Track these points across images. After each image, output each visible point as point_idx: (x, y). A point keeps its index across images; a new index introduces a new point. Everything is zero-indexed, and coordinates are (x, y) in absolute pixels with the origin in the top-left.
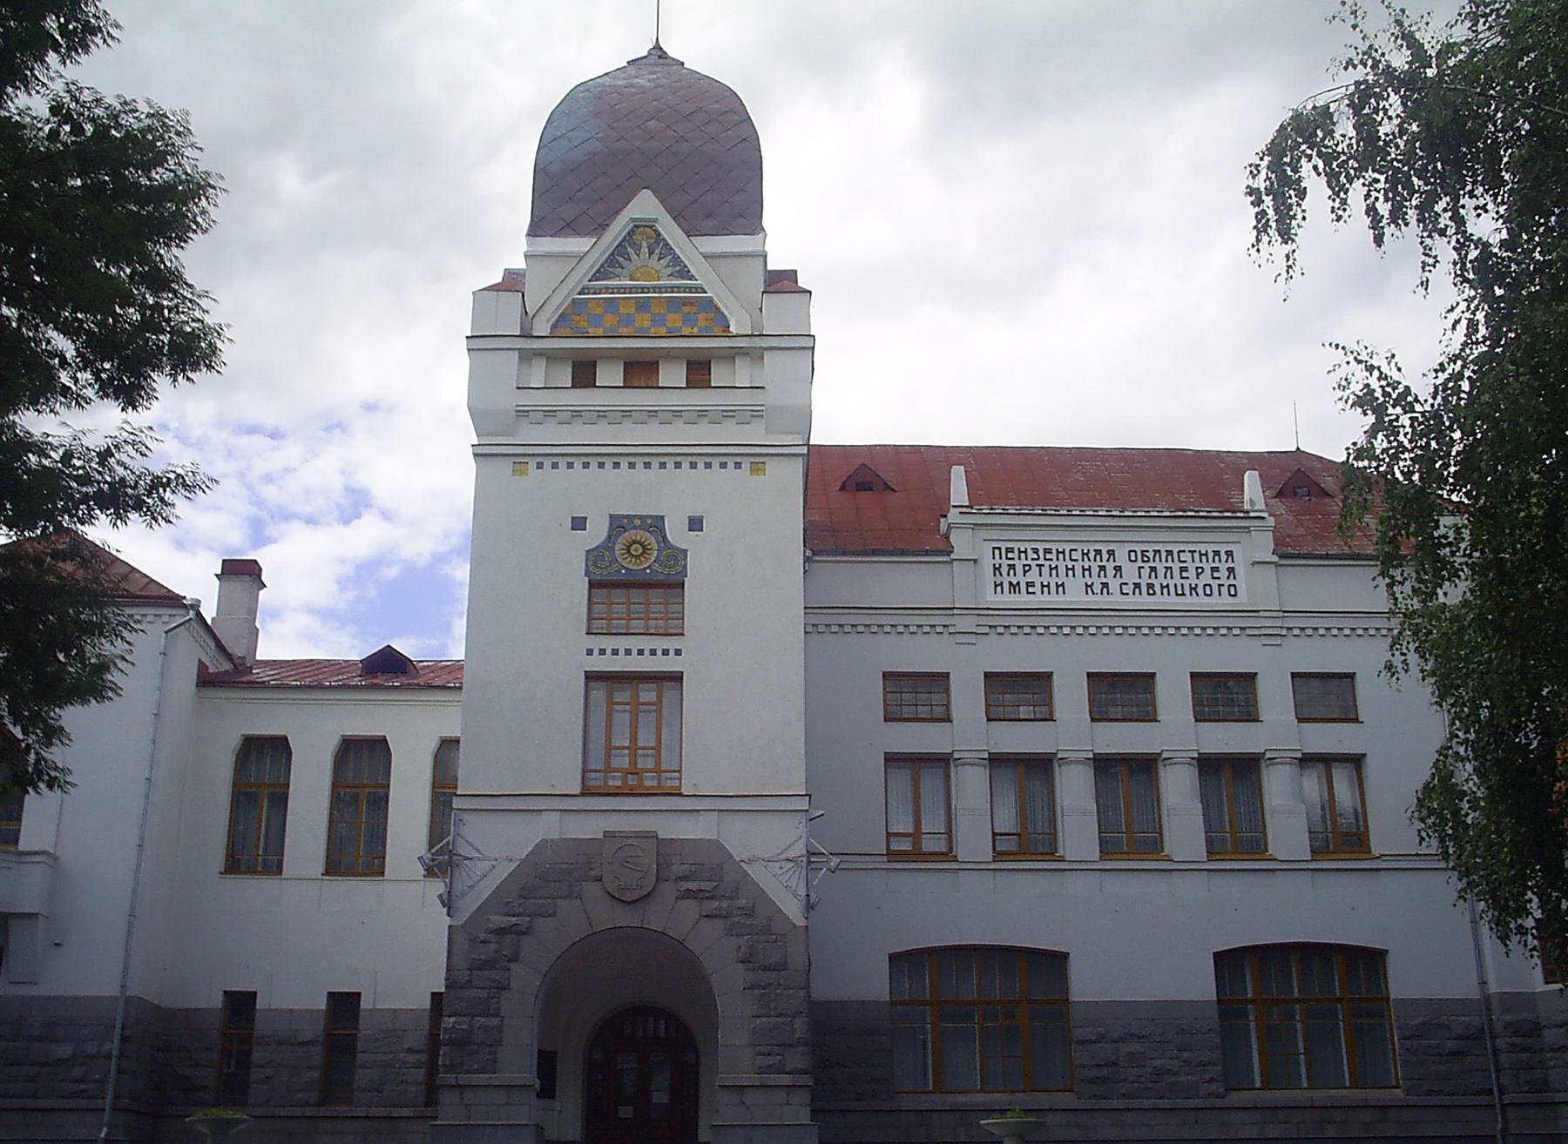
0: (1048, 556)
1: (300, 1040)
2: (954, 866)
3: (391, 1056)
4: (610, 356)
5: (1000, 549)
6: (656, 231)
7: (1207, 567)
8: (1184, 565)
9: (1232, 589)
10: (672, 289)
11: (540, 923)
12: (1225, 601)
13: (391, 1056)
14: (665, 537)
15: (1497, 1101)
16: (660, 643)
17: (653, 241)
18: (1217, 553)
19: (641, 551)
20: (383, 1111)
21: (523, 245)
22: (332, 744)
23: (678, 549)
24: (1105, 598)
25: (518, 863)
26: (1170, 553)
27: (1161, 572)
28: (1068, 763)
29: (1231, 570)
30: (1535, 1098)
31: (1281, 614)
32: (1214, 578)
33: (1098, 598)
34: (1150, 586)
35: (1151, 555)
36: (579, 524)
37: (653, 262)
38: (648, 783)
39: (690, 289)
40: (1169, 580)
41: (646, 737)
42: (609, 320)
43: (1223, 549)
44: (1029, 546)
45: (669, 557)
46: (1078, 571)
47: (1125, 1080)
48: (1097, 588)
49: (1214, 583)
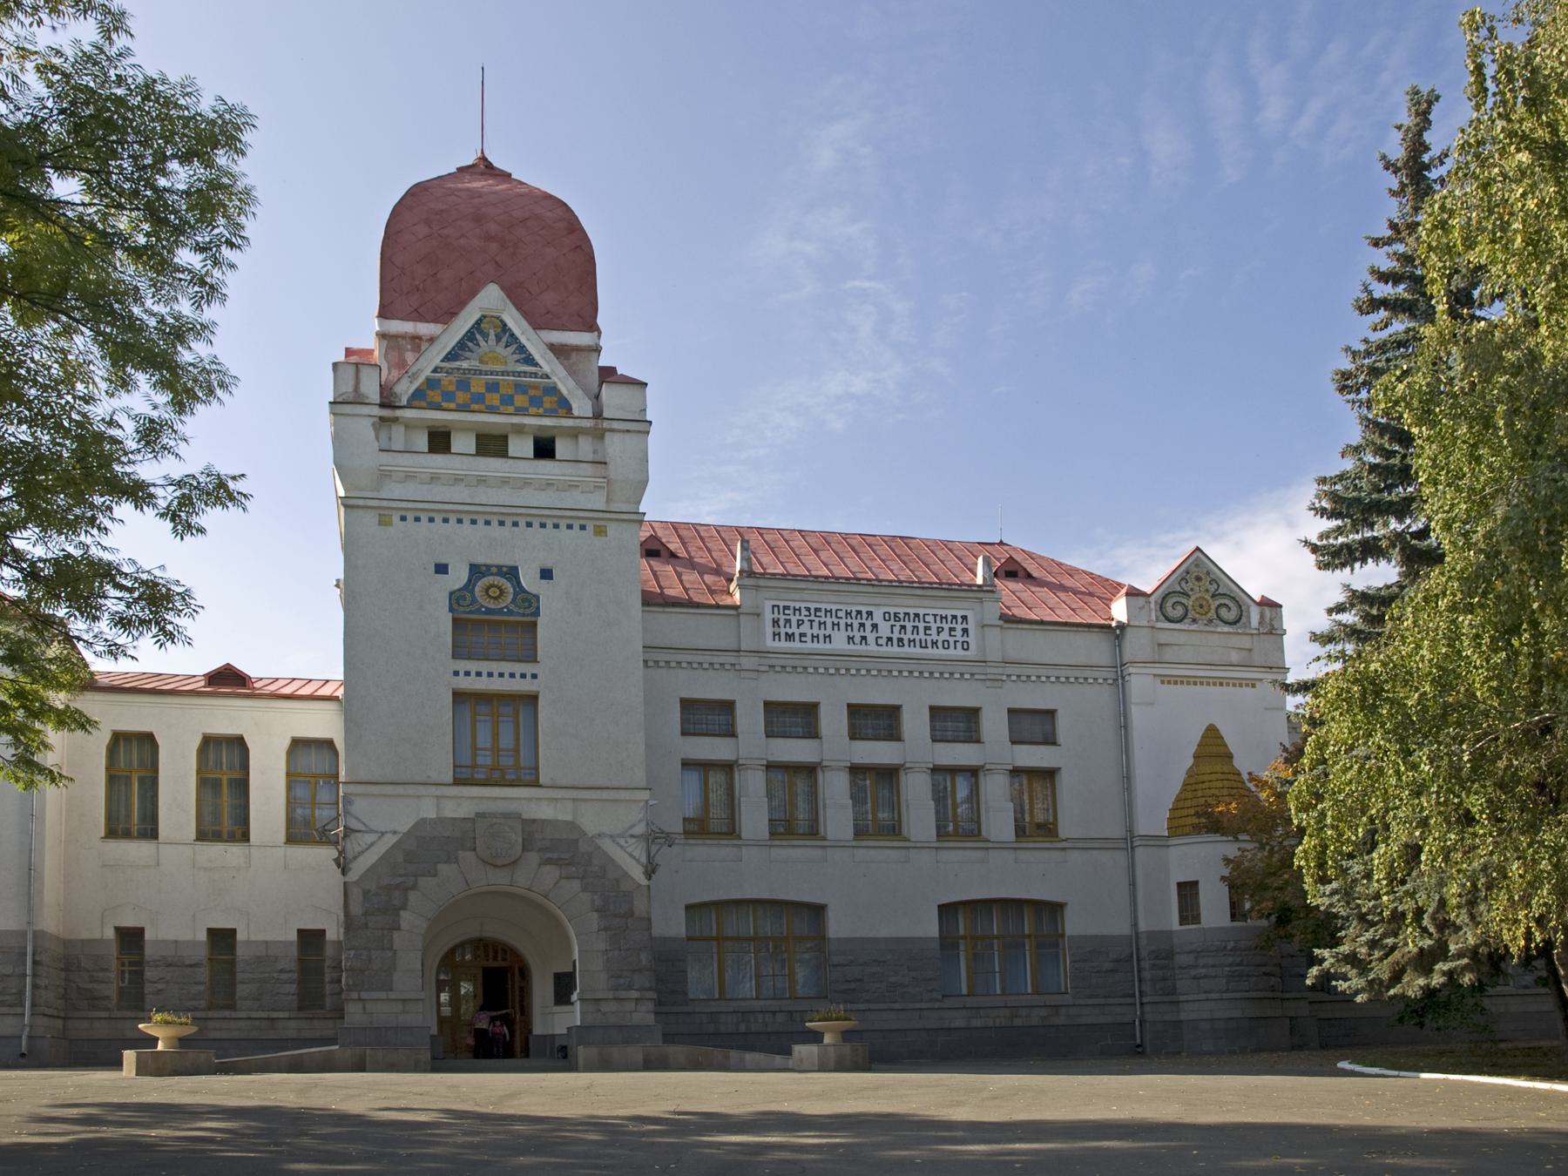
0: (818, 614)
1: (187, 962)
2: (739, 842)
3: (267, 975)
4: (465, 428)
5: (778, 606)
6: (502, 321)
7: (946, 627)
8: (788, 617)
9: (965, 644)
10: (519, 374)
11: (422, 881)
12: (959, 652)
13: (267, 975)
14: (519, 583)
15: (1138, 1000)
16: (518, 668)
17: (499, 330)
18: (954, 617)
19: (498, 593)
20: (264, 1015)
21: (376, 325)
22: (286, 743)
23: (460, 590)
24: (863, 647)
25: (401, 835)
26: (917, 615)
27: (909, 629)
28: (832, 770)
29: (965, 631)
30: (1166, 999)
31: (1003, 665)
32: (950, 635)
33: (858, 647)
34: (900, 640)
35: (902, 616)
36: (442, 569)
37: (500, 349)
38: (508, 777)
39: (535, 375)
40: (915, 636)
41: (506, 741)
42: (461, 397)
43: (864, 609)
44: (803, 605)
45: (524, 601)
46: (842, 626)
47: (868, 991)
48: (857, 640)
49: (952, 640)
